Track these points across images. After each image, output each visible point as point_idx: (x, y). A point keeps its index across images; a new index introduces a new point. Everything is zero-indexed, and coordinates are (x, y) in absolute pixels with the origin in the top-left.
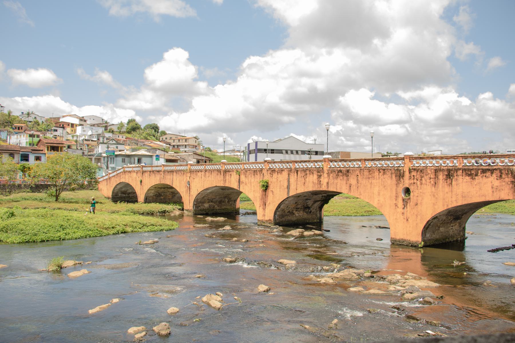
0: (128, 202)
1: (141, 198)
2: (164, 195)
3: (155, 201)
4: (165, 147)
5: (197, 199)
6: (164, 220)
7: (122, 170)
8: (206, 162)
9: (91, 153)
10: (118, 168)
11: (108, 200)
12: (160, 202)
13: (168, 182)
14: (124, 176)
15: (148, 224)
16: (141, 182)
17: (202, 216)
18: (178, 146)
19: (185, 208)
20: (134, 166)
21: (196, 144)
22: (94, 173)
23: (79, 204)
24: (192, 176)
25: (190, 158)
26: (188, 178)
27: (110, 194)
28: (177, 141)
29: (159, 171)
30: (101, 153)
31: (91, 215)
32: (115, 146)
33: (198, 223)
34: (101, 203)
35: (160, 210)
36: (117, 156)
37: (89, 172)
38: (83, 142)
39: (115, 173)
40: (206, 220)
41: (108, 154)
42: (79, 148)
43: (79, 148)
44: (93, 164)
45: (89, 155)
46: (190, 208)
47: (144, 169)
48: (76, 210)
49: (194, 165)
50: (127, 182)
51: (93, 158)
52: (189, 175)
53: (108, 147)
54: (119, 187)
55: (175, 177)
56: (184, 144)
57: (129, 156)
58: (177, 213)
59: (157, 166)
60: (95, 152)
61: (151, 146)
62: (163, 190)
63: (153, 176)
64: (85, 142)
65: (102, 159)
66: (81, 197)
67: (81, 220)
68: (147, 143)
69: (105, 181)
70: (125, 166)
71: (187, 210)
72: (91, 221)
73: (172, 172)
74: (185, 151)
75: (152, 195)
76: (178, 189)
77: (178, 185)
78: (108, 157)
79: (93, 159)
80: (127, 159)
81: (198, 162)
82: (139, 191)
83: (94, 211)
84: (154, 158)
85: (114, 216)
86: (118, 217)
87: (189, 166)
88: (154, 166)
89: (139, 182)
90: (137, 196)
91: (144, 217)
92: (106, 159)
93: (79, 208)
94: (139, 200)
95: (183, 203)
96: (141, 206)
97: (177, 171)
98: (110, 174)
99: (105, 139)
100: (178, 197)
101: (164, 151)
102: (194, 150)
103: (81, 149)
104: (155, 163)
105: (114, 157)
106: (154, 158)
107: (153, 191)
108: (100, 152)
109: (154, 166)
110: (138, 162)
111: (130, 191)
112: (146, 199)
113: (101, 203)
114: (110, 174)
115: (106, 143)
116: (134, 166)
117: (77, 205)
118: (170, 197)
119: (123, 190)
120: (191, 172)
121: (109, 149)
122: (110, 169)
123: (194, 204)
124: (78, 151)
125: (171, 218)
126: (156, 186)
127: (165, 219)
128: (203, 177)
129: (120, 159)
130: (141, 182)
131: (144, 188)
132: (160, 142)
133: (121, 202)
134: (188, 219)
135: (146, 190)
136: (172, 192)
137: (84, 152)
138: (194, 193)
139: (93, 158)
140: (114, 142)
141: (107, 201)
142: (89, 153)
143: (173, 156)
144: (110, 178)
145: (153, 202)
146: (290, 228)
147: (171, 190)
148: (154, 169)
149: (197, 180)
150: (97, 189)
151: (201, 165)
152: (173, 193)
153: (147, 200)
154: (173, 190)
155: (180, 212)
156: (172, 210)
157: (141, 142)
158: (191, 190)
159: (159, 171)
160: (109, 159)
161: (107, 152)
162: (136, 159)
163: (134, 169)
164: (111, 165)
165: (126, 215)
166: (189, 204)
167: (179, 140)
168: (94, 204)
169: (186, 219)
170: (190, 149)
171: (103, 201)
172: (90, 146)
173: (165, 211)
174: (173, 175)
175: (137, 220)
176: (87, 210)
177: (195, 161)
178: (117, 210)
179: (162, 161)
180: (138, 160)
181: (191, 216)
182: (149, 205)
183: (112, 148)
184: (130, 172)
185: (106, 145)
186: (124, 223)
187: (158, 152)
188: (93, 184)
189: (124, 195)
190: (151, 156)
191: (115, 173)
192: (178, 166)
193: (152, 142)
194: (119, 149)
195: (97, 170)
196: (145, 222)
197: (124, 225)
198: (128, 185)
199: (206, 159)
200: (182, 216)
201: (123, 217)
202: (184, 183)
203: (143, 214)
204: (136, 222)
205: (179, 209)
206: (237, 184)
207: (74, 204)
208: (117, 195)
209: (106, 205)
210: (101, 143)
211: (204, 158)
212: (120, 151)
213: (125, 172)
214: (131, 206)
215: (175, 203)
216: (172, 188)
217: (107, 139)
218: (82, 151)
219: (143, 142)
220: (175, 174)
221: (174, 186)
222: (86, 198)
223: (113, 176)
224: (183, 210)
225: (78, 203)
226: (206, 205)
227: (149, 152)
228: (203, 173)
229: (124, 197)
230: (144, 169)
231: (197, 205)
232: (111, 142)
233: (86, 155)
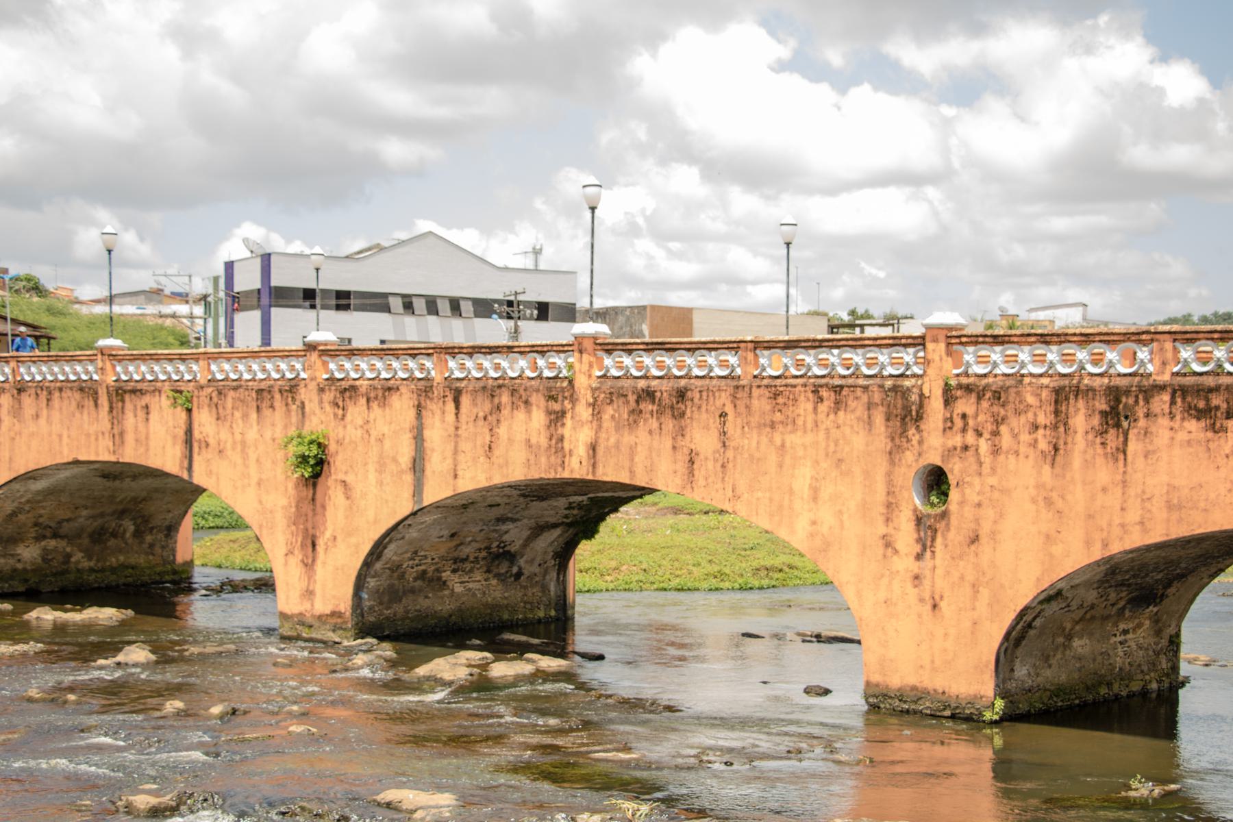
126: (1042, 597)
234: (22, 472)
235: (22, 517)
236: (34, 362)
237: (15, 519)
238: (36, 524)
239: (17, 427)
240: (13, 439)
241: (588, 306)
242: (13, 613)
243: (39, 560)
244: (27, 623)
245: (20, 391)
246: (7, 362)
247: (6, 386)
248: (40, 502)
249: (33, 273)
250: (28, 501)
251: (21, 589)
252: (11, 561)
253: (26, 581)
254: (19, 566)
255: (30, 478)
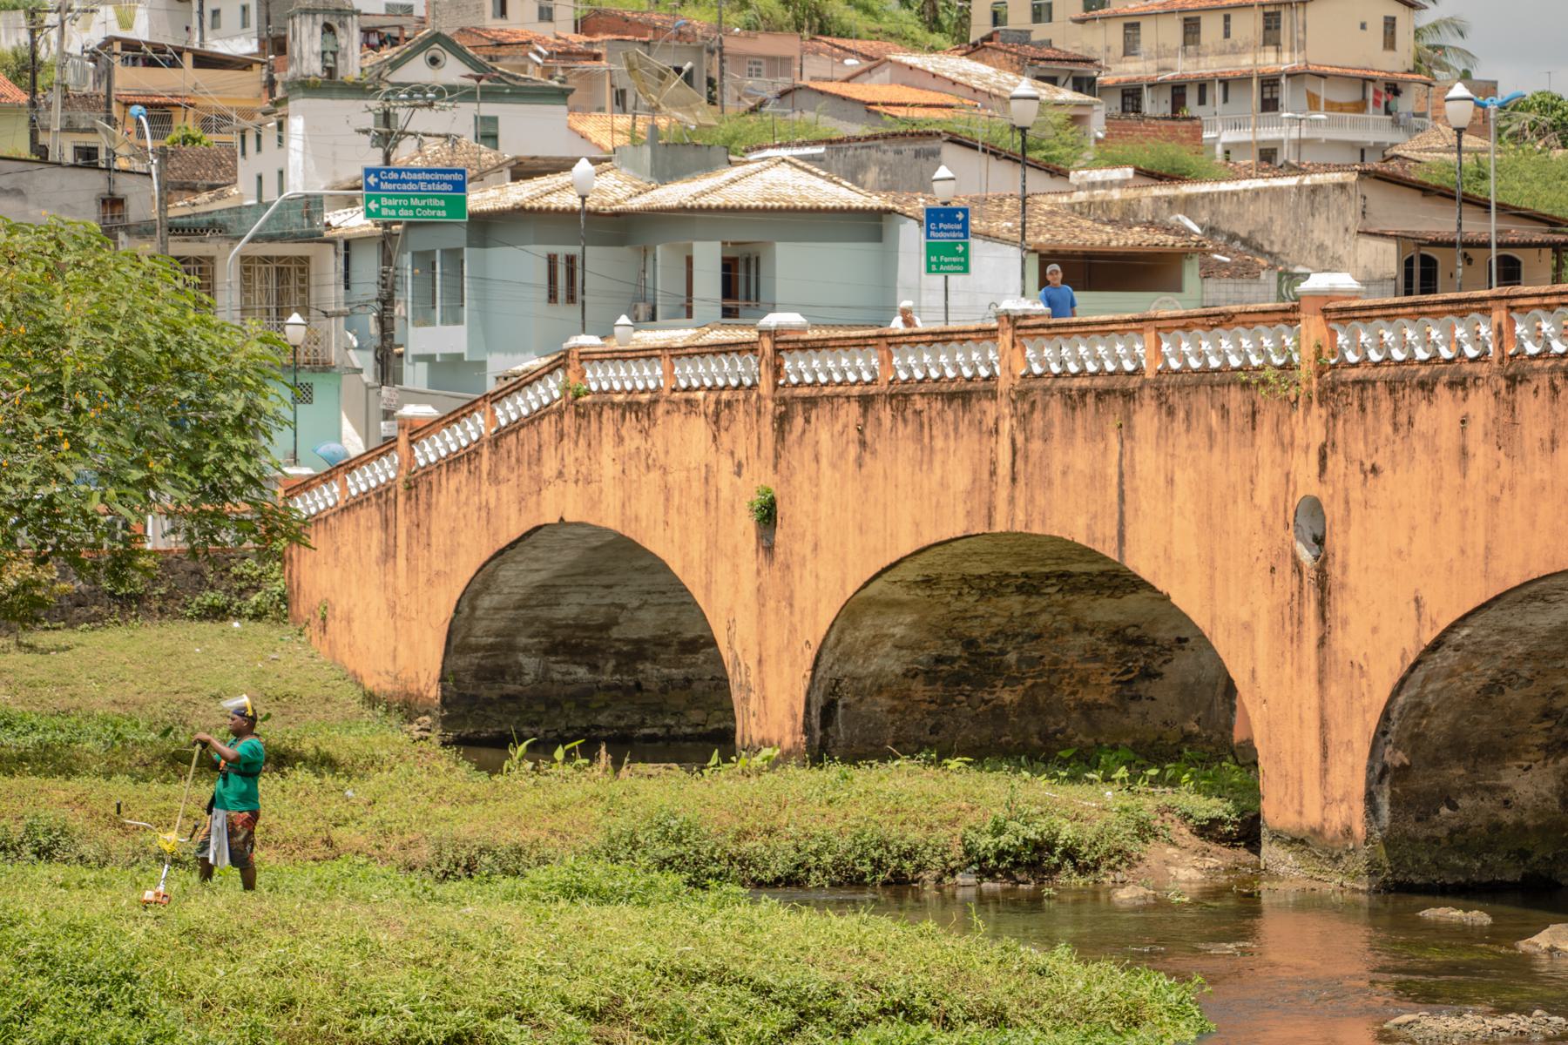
0: (628, 746)
1: (771, 701)
2: (1035, 662)
3: (930, 739)
4: (1024, 114)
5: (1419, 708)
6: (1034, 955)
7: (550, 390)
8: (1510, 271)
9: (204, 203)
10: (500, 364)
11: (399, 736)
12: (982, 753)
13: (1070, 515)
14: (573, 452)
15: (855, 1003)
16: (768, 515)
17: (1479, 917)
18: (1178, 92)
19: (1276, 812)
20: (680, 335)
21: (1394, 63)
22: (240, 426)
23: (77, 785)
24: (1355, 441)
25: (1321, 230)
26: (1305, 468)
27: (420, 661)
28: (1172, 31)
29: (962, 395)
30: (311, 205)
31: (220, 903)
32: (461, 118)
33: (1429, 997)
34: (325, 763)
35: (985, 842)
36: (486, 227)
37: (192, 426)
38: (106, 75)
39: (475, 427)
40: (1524, 966)
41: (389, 207)
42: (63, 147)
43: (63, 147)
44: (230, 322)
45: (179, 229)
46: (1337, 819)
47: (799, 368)
48: (44, 853)
49: (1366, 314)
50: (612, 522)
51: (228, 260)
52: (1310, 427)
53: (387, 135)
54: (516, 579)
55: (1147, 459)
56: (1246, 63)
57: (621, 227)
58: (1186, 870)
59: (942, 338)
60: (242, 192)
61: (868, 108)
62: (1014, 603)
63: (896, 445)
64: (128, 79)
65: (328, 265)
66: (99, 699)
67: (102, 959)
68: (818, 69)
69: (370, 515)
70: (590, 341)
71: (1297, 842)
72: (210, 974)
73: (1116, 393)
74: (1268, 155)
75: (889, 663)
76: (1187, 597)
77: (1187, 546)
78: (386, 244)
79: (228, 275)
80: (601, 265)
81: (1421, 272)
82: (745, 628)
83: (242, 860)
84: (911, 238)
85: (474, 909)
86: (508, 916)
87: (1312, 328)
88: (914, 340)
89: (746, 524)
90: (721, 683)
91: (809, 917)
92: (368, 267)
93: (78, 821)
94: (748, 727)
95: (1247, 758)
96: (770, 793)
97: (1174, 391)
98: (418, 432)
99: (350, 40)
100: (1188, 692)
101: (1020, 159)
102: (1372, 129)
103: (87, 157)
104: (922, 296)
105: (458, 238)
106: (911, 238)
107: (899, 626)
108: (296, 185)
109: (914, 340)
110: (729, 290)
111: (646, 623)
112: (828, 712)
113: (325, 763)
114: (418, 432)
115: (357, 90)
116: (680, 335)
117: (59, 789)
118: (1102, 688)
119: (569, 609)
120: (1337, 388)
121: (405, 154)
122: (415, 376)
123: (1379, 773)
124: (47, 180)
125: (1104, 938)
126: (935, 564)
127: (1050, 943)
128: (1482, 453)
129: (520, 266)
130: (768, 515)
131: (805, 592)
132: (975, 50)
133: (541, 749)
134: (1314, 941)
135: (827, 615)
136: (1117, 634)
137: (124, 187)
138: (1382, 637)
139: (228, 260)
140: (453, 72)
141: (394, 737)
142: (180, 208)
143: (1126, 216)
144: (416, 483)
145: (908, 746)
146: (1551, 915)
147: (1105, 610)
148: (912, 365)
149: (1408, 484)
150: (282, 609)
151: (1461, 308)
152: (1128, 639)
153: (839, 727)
154: (1133, 603)
155: (1221, 858)
156: (1124, 836)
157: (757, 64)
158: (1342, 606)
159: (962, 395)
160: (406, 261)
161: (378, 182)
162: (708, 258)
163: (690, 373)
164: (425, 339)
165: (602, 897)
166: (1315, 764)
167: (1191, 28)
168: (248, 770)
169: (1286, 944)
170: (1325, 126)
171: (342, 744)
172: (184, 124)
173: (1043, 847)
174: (1126, 429)
175: (725, 950)
176: (170, 840)
177: (1385, 258)
178: (511, 836)
179: (998, 281)
180: (729, 266)
181: (1344, 911)
182: (866, 777)
183: (436, 134)
184: (638, 408)
185: (362, 113)
186: (580, 992)
187: (952, 177)
188: (235, 564)
189: (581, 669)
190: (871, 225)
191: (475, 427)
192: (1186, 324)
193: (874, 63)
194: (514, 145)
195: (276, 398)
196: (819, 979)
197: (588, 1013)
198: (618, 556)
199: (1519, 231)
200: (1235, 910)
201: (567, 916)
202: (1256, 528)
203: (790, 883)
204: (721, 977)
205: (1208, 830)
206: (1115, 544)
207: (26, 782)
208: (497, 674)
209: (376, 781)
210: (307, 87)
211: (1487, 228)
212: (522, 171)
213: (582, 408)
214: (658, 790)
215: (1155, 754)
216: (1119, 581)
217: (375, 37)
218: (94, 183)
219: (779, 64)
220: (1146, 418)
221: (1140, 563)
222: (160, 710)
223: (452, 462)
224: (1249, 833)
225: (68, 770)
226: (1529, 785)
227: (853, 175)
228: (1480, 404)
229: (583, 698)
230: (799, 368)
231: (1423, 782)
232: (417, 71)
233: (144, 231)
234: (1516, 582)
235: (1514, 695)
236: (1549, 308)
237: (1497, 700)
238: (1547, 714)
239: (1505, 472)
240: (1497, 500)
241: (952, 278)
242: (1493, 935)
243: (1556, 804)
244: (1528, 958)
245: (1513, 381)
246: (1485, 311)
247: (1482, 369)
248: (1556, 657)
249: (1556, 91)
250: (1528, 656)
251: (1512, 875)
252: (1488, 805)
253: (1524, 855)
254: (1508, 817)
255: (1533, 597)
